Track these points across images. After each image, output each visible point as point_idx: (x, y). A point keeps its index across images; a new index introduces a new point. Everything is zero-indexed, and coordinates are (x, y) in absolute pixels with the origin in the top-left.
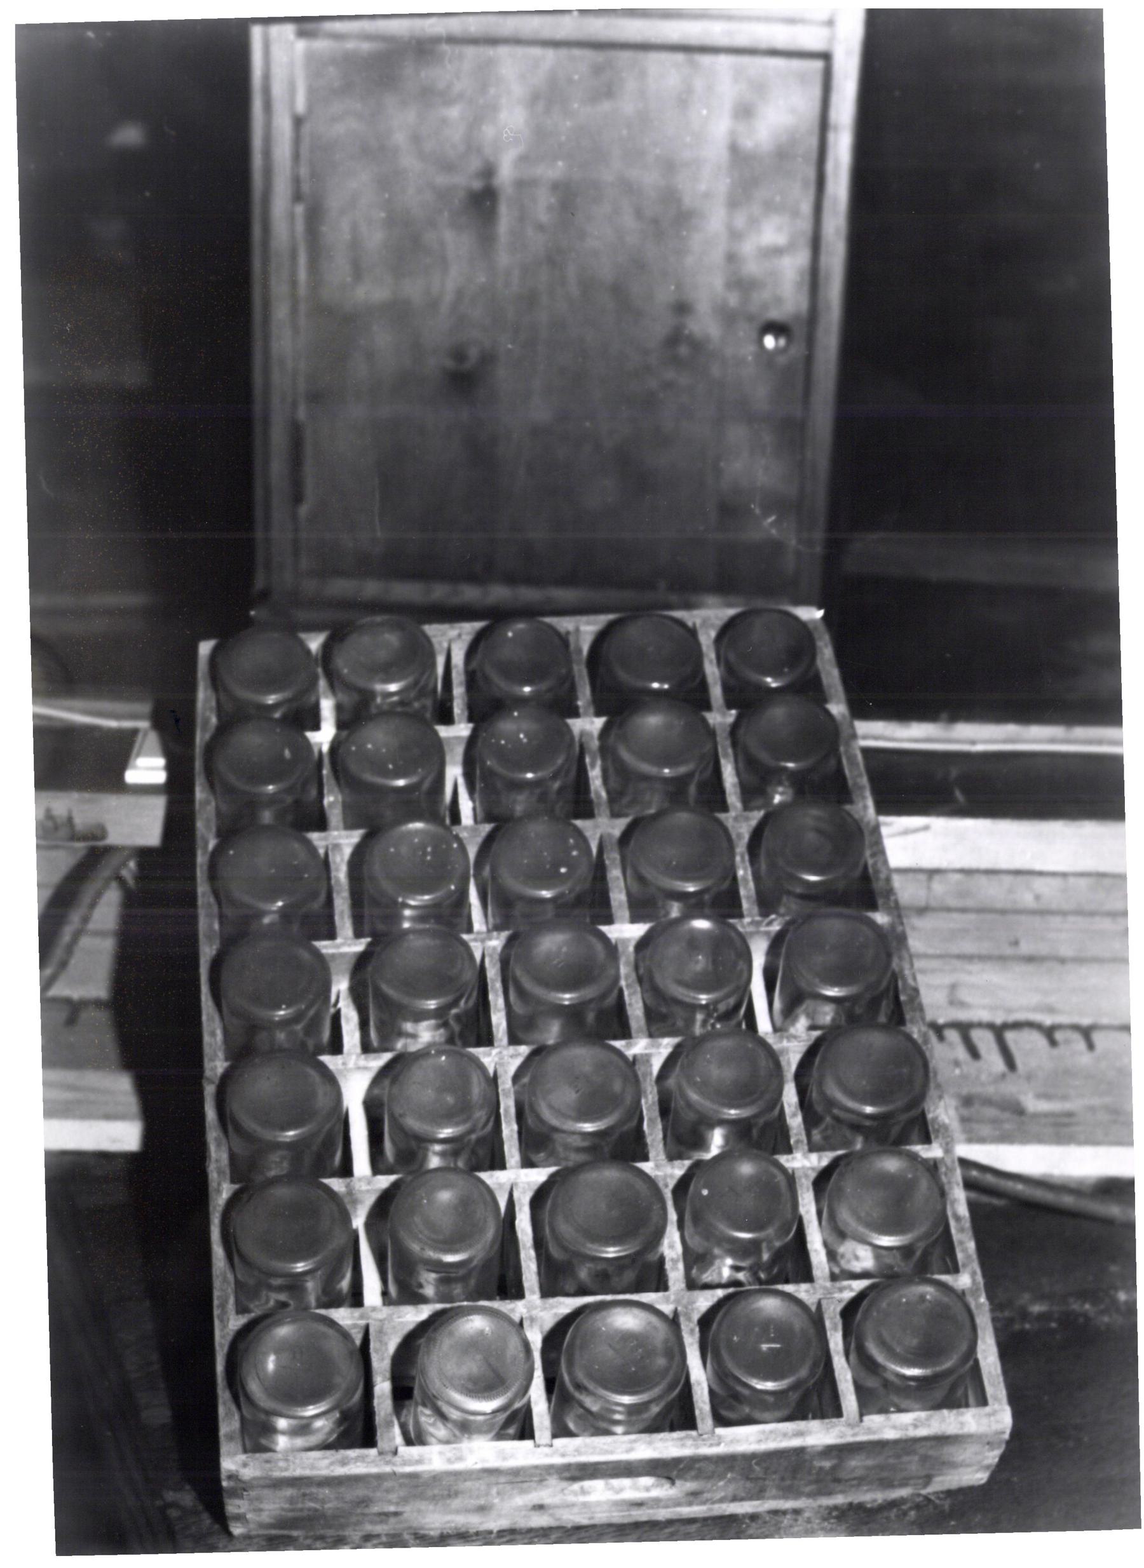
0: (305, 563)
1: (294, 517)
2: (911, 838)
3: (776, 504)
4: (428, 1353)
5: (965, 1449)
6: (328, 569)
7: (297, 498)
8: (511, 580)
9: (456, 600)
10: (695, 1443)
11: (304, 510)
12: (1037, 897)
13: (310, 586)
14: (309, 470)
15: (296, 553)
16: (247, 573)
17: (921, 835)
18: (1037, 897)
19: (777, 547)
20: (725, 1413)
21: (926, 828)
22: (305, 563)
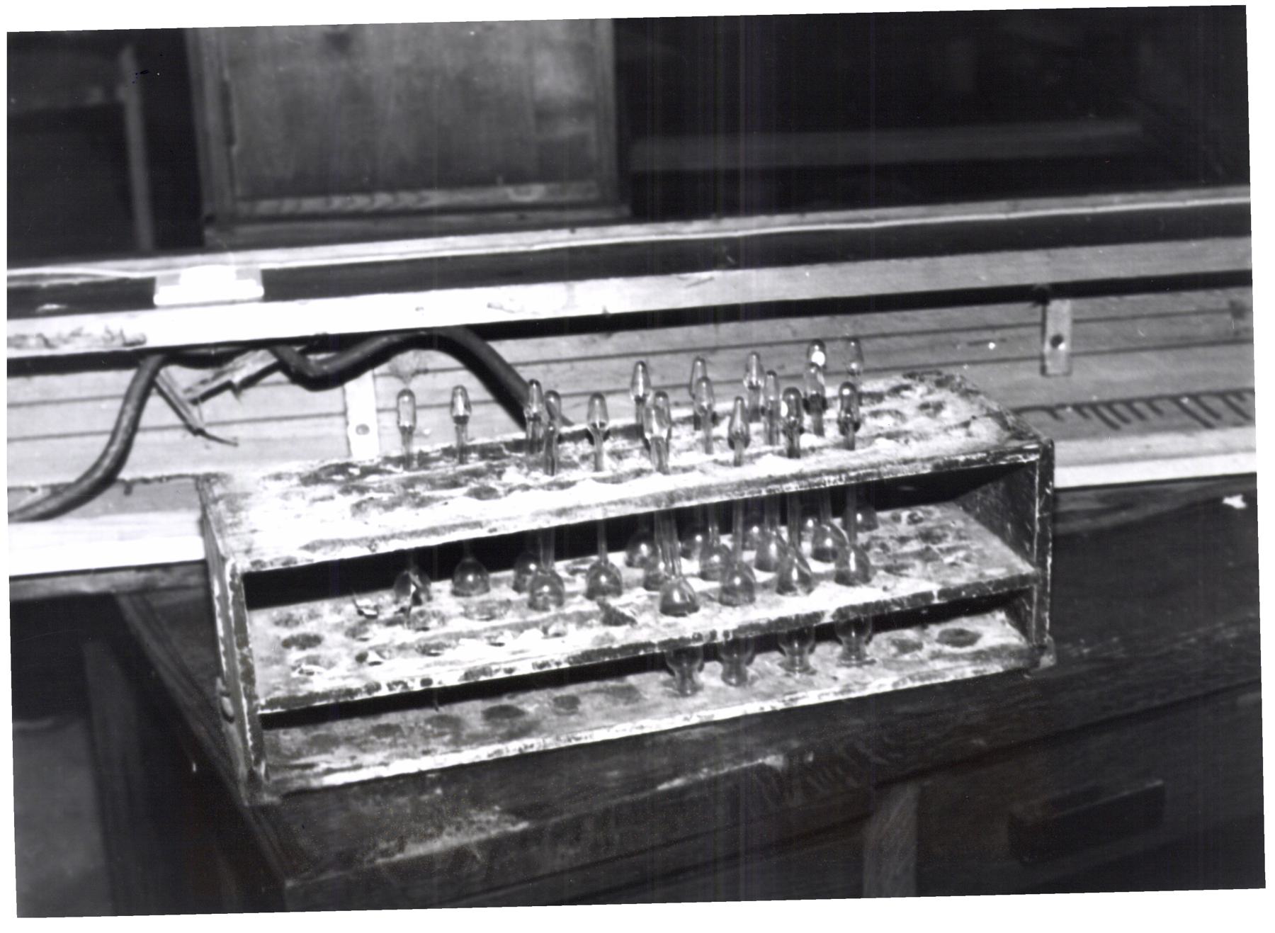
0: (239, 191)
1: (228, 155)
2: (702, 287)
3: (581, 109)
4: (107, 512)
5: (435, 842)
6: (257, 193)
7: (230, 141)
8: (391, 188)
9: (351, 207)
10: (700, 434)
11: (235, 149)
12: (794, 333)
13: (244, 208)
14: (235, 106)
15: (232, 185)
16: (195, 199)
17: (708, 284)
18: (794, 333)
19: (582, 140)
20: (650, 584)
21: (711, 279)
22: (239, 191)
